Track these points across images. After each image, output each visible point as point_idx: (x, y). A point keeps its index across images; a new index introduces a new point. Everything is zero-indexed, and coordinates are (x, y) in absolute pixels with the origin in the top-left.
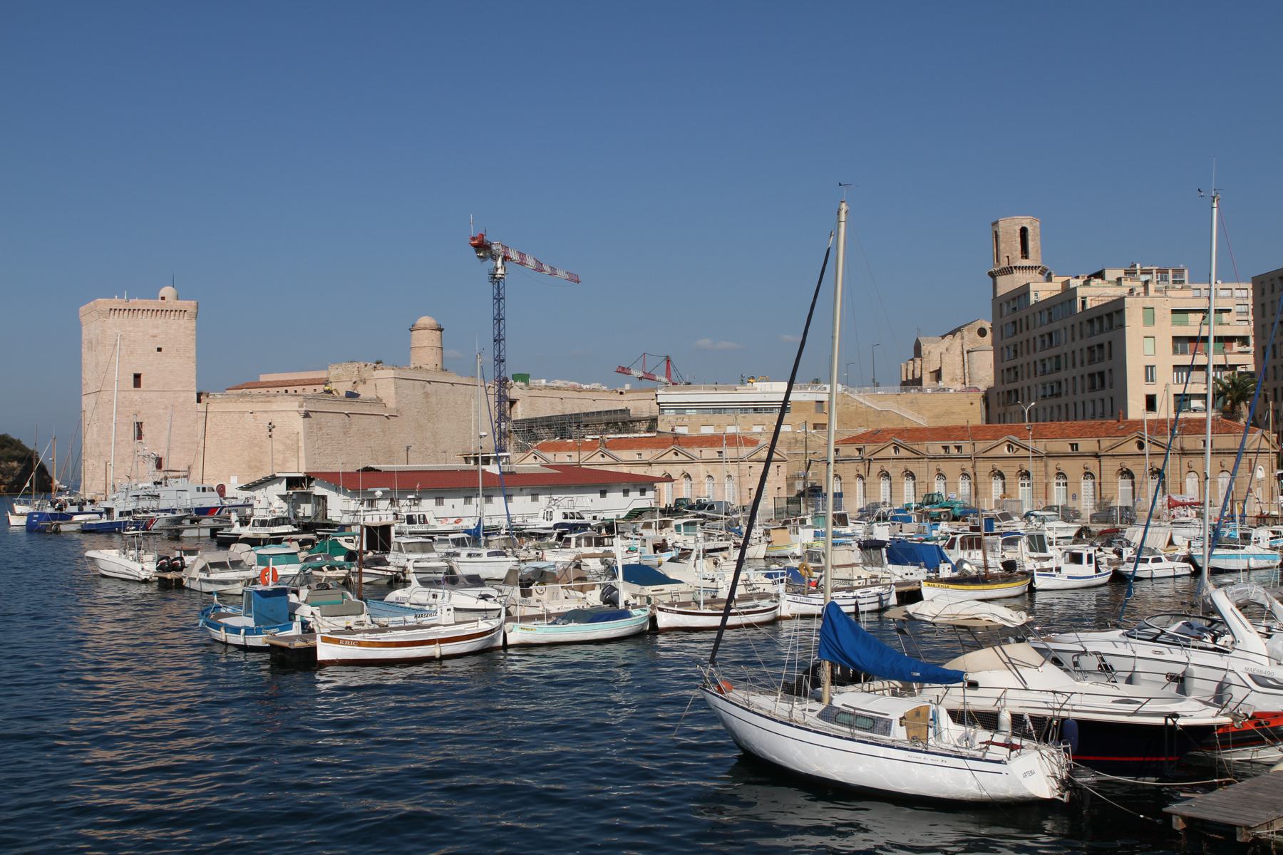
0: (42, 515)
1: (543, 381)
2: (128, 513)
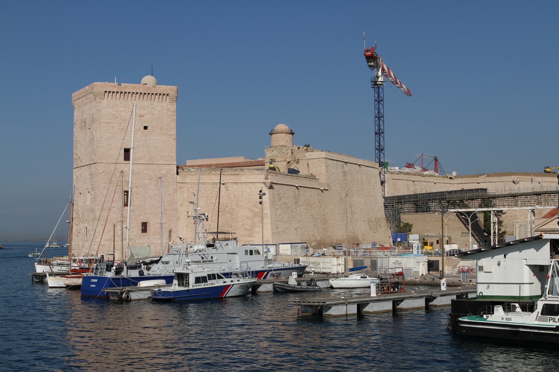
0: (102, 280)
1: (397, 168)
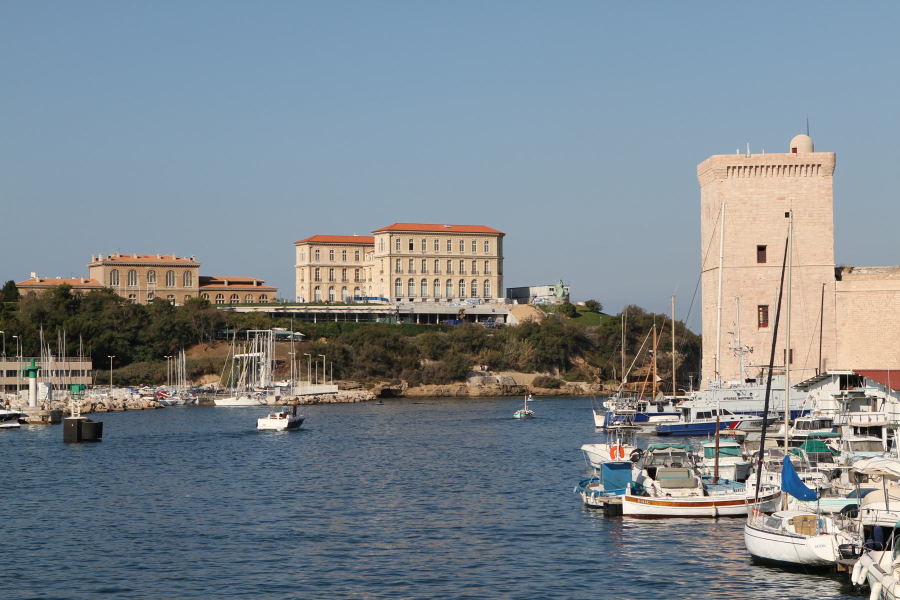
2: (708, 415)
